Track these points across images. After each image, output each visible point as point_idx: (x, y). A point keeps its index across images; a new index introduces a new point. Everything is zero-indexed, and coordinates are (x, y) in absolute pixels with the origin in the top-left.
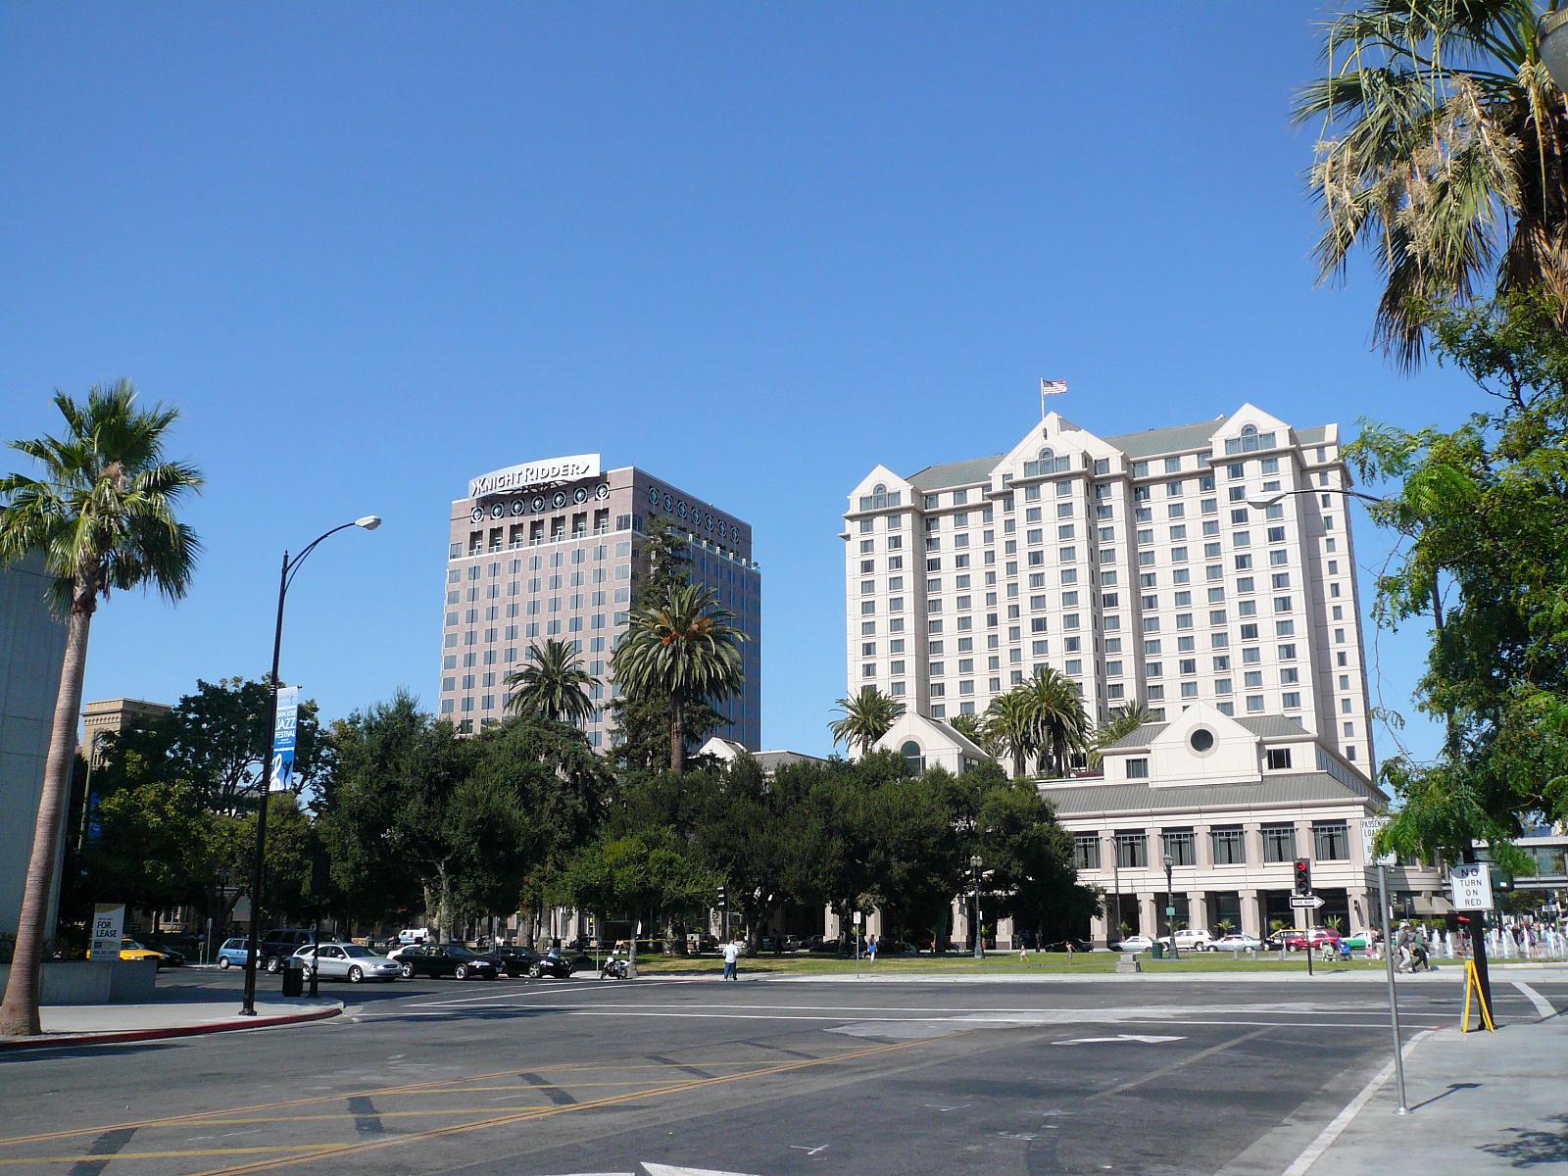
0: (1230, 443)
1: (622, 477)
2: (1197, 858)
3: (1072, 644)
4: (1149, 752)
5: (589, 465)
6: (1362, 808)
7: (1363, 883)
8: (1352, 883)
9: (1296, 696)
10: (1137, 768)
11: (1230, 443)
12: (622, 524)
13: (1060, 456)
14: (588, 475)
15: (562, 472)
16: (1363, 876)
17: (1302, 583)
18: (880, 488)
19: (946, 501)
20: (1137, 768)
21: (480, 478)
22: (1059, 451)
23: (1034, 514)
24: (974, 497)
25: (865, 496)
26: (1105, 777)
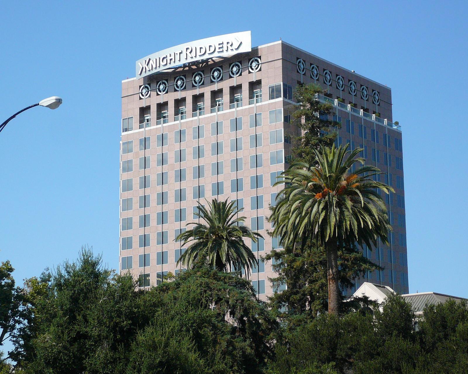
15: (217, 50)
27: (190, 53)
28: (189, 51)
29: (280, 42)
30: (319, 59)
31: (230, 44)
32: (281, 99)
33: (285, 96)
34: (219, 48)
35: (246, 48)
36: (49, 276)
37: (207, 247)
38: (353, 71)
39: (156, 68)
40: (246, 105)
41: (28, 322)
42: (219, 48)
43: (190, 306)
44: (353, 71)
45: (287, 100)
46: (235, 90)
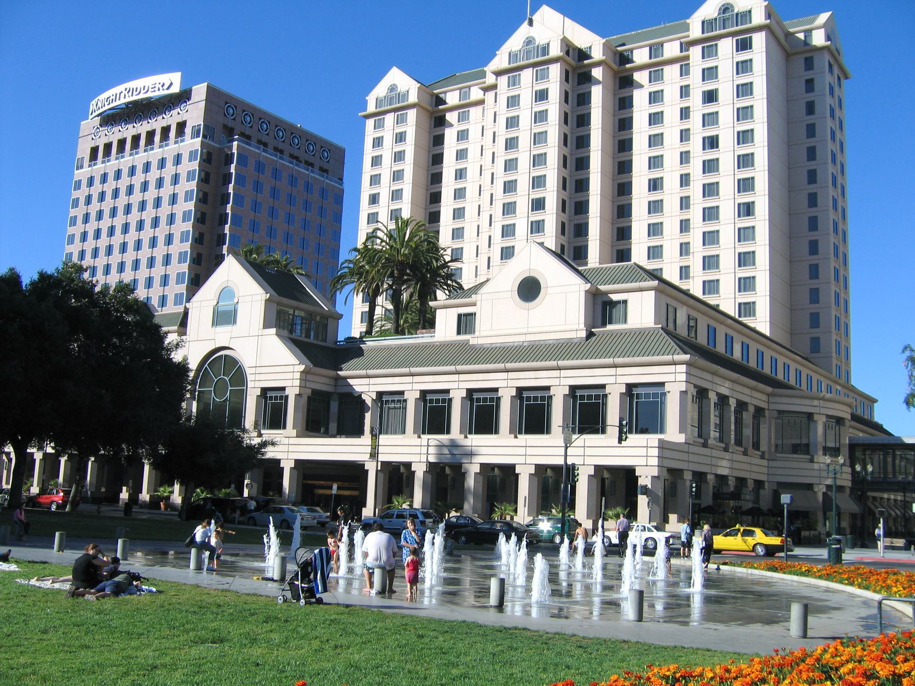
0: (379, 102)
1: (200, 92)
2: (637, 596)
3: (746, 284)
4: (474, 305)
5: (172, 82)
6: (683, 368)
7: (655, 461)
8: (642, 461)
9: (541, 223)
10: (465, 323)
11: (379, 102)
12: (196, 134)
13: (741, 10)
14: (172, 91)
15: (150, 90)
16: (655, 452)
17: (414, 139)
18: (393, 88)
19: (641, 56)
20: (465, 323)
21: (94, 101)
22: (740, 6)
23: (710, 73)
24: (671, 49)
25: (707, 18)
26: (436, 334)
27: (128, 92)
28: (128, 90)
29: (206, 84)
30: (281, 121)
31: (162, 84)
32: (200, 139)
33: (204, 137)
34: (152, 88)
35: (176, 89)
36: (743, 535)
37: (848, 531)
38: (299, 126)
39: (102, 107)
40: (172, 145)
41: (121, 492)
42: (152, 88)
43: (573, 550)
44: (299, 126)
45: (207, 141)
46: (166, 131)
